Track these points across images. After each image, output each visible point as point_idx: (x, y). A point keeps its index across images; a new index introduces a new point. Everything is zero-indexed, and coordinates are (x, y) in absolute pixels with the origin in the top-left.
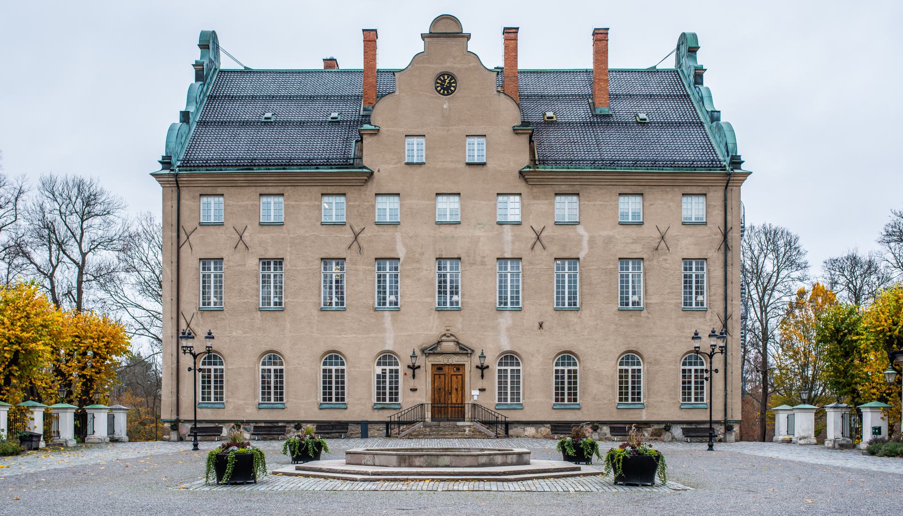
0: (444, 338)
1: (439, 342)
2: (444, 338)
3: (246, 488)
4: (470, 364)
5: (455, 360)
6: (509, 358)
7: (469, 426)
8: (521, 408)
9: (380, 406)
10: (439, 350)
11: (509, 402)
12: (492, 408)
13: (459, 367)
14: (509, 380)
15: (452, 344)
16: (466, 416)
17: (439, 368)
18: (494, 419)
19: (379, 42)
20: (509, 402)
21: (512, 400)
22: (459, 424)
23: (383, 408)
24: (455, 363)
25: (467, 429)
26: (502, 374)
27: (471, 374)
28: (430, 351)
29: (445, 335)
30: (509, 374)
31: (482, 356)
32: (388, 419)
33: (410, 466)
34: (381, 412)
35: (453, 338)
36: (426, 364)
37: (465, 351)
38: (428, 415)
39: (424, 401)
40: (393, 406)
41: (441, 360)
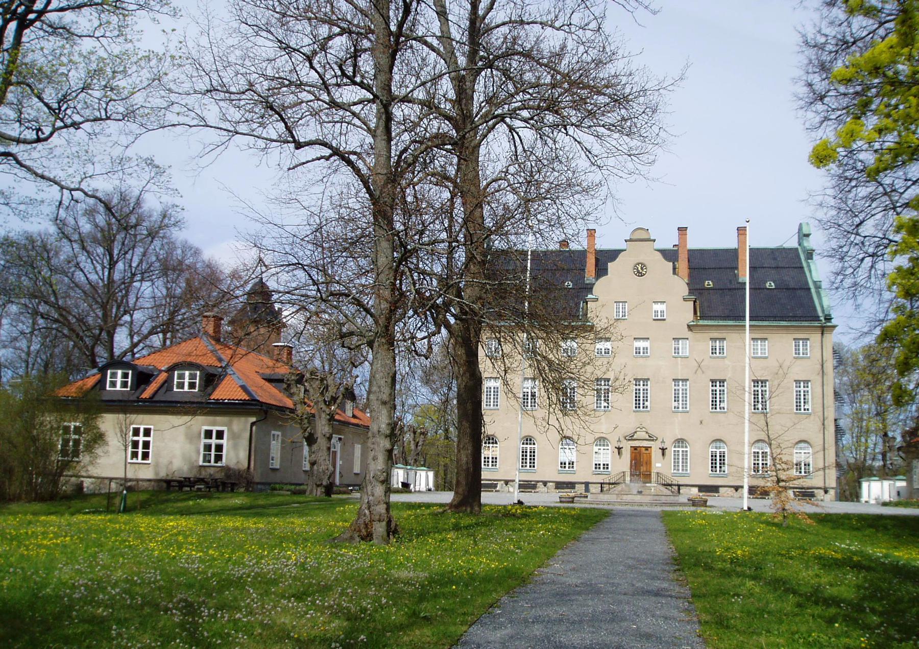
4: (655, 447)
5: (646, 444)
6: (680, 442)
10: (635, 437)
13: (647, 448)
14: (681, 457)
27: (656, 454)
28: (631, 438)
31: (663, 442)
36: (627, 446)
37: (651, 438)
38: (628, 478)
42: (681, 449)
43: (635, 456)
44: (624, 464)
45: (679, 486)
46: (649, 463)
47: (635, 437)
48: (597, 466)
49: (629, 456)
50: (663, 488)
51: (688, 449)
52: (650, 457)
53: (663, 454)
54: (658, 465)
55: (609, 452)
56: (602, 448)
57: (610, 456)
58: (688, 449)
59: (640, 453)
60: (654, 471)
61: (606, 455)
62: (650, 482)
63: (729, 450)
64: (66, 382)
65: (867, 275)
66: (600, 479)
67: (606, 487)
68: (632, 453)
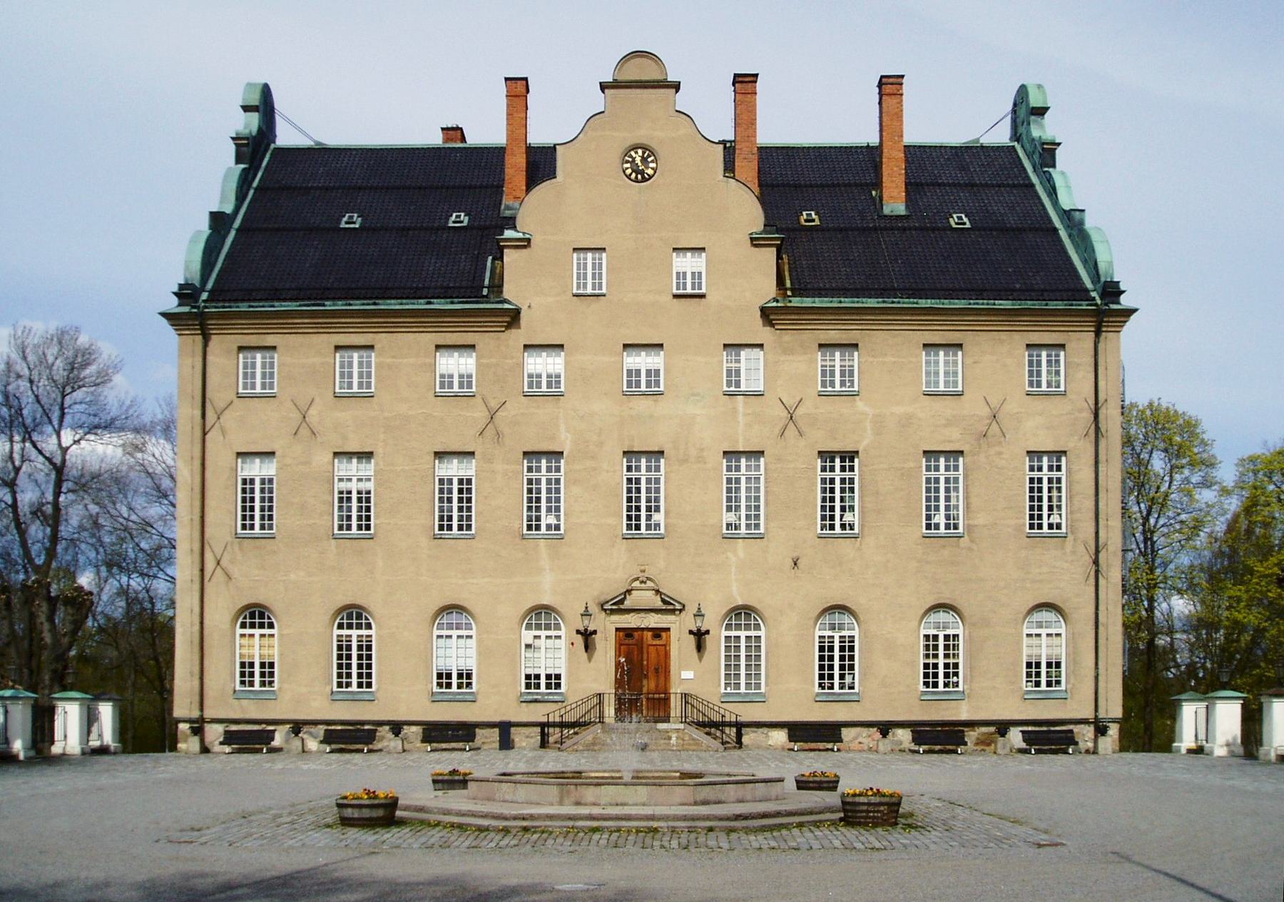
0: (636, 584)
1: (629, 591)
2: (636, 584)
4: (679, 627)
5: (653, 621)
6: (742, 614)
10: (628, 604)
11: (743, 690)
13: (658, 632)
14: (743, 653)
16: (672, 714)
17: (626, 634)
20: (743, 690)
21: (748, 685)
22: (661, 726)
23: (536, 701)
27: (681, 645)
28: (617, 606)
29: (637, 579)
30: (743, 644)
31: (699, 614)
35: (649, 584)
36: (606, 627)
37: (670, 606)
38: (610, 711)
42: (743, 634)
44: (598, 676)
45: (740, 726)
46: (663, 670)
47: (628, 604)
50: (699, 735)
51: (762, 633)
52: (667, 655)
53: (700, 647)
54: (687, 674)
55: (562, 643)
56: (543, 633)
57: (563, 654)
58: (762, 633)
59: (640, 645)
60: (676, 689)
62: (666, 719)
66: (538, 713)
67: (554, 734)
68: (619, 645)
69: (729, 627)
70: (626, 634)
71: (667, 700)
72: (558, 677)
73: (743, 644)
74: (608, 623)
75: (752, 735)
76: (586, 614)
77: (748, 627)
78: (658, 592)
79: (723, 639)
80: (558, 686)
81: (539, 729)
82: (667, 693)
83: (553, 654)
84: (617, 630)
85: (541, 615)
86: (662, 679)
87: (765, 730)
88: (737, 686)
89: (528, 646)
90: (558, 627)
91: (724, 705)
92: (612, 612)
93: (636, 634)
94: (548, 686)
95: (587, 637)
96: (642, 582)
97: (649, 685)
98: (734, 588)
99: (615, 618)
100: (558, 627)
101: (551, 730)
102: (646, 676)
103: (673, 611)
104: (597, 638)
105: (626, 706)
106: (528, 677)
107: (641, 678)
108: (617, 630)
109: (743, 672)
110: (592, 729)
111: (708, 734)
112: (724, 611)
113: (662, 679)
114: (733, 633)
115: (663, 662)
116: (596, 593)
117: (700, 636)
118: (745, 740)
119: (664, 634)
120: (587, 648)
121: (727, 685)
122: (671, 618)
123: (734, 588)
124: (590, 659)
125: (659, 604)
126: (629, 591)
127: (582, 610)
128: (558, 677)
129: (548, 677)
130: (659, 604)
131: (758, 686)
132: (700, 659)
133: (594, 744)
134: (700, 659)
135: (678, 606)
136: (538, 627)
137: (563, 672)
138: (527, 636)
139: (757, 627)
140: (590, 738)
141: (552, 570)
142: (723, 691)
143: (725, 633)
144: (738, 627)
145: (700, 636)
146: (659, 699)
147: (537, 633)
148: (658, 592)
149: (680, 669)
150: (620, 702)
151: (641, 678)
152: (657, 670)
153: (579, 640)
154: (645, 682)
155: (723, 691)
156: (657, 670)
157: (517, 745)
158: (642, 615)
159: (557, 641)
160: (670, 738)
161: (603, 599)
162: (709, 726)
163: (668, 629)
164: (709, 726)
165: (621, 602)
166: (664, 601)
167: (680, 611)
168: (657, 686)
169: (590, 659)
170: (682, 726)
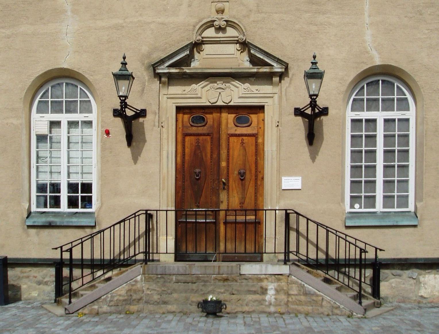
0: (210, 33)
1: (196, 46)
2: (210, 33)
3: (329, 109)
4: (279, 103)
5: (237, 94)
6: (381, 80)
7: (278, 276)
8: (412, 223)
9: (41, 220)
10: (197, 64)
11: (379, 207)
12: (337, 225)
13: (246, 112)
14: (380, 148)
15: (233, 49)
16: (269, 247)
17: (193, 115)
18: (354, 254)
19: (67, 148)
20: (379, 207)
21: (388, 199)
22: (249, 269)
23: (50, 226)
24: (236, 101)
25: (271, 287)
26: (364, 130)
27: (279, 132)
28: (177, 69)
29: (210, 24)
30: (380, 132)
31: (314, 75)
32: (56, 255)
33: (47, 188)
34: (46, 232)
35: (231, 32)
36: (162, 104)
37: (264, 69)
38: (166, 242)
39: (152, 205)
40: (75, 221)
41: (203, 94)
42: (380, 116)
43: (198, 149)
44: (144, 184)
45: (378, 266)
46: (252, 175)
47: (197, 64)
48: (49, 193)
49: (170, 148)
50: (312, 282)
51: (411, 114)
52: (259, 152)
53: (312, 137)
54: (294, 181)
55: (94, 134)
56: (64, 118)
57: (94, 152)
58: (411, 114)
59: (215, 136)
60: (273, 203)
61: (82, 151)
62: (257, 257)
63: (420, 121)
64: (216, 256)
65: (74, 31)
66: (45, 245)
67: (80, 278)
68: (182, 135)
69: (357, 105)
70: (193, 115)
71: (257, 225)
72: (87, 187)
73: (380, 132)
74: (164, 99)
75: (394, 281)
76: (123, 76)
77: (388, 105)
78: (245, 45)
79: (348, 124)
80: (87, 202)
81: (52, 271)
82: (257, 210)
83: (82, 151)
84: (180, 109)
85: (57, 84)
86: (251, 190)
87: (415, 272)
88: (371, 200)
89: (41, 138)
90: (87, 108)
91: (349, 232)
92: (171, 79)
93: (209, 118)
94: (72, 203)
95: (131, 122)
96: (220, 29)
97: (230, 199)
98: (368, 38)
99: (176, 90)
100: (87, 108)
101: (77, 272)
102: (226, 186)
103: (267, 78)
104: (148, 122)
105: (195, 235)
106: (41, 188)
107: (215, 203)
108: (180, 109)
109: (380, 178)
110: (130, 271)
111: (327, 281)
112: (353, 74)
113: (251, 190)
114: (365, 115)
115: (252, 159)
116: (145, 49)
117: (312, 117)
118: (384, 288)
119: (254, 118)
120: (130, 139)
121: (354, 199)
122: (266, 89)
123: (368, 38)
124: (135, 158)
125: (243, 63)
126: (196, 46)
127: (116, 68)
128: (87, 187)
129: (72, 187)
130: (243, 63)
131: (404, 201)
132: (313, 157)
133: (129, 301)
134: (313, 157)
135: (278, 68)
136: (57, 108)
137: (94, 180)
138: (40, 123)
139: (403, 104)
140: (122, 291)
141: (75, 12)
142: (348, 209)
143: (351, 115)
144: (373, 104)
145: (312, 117)
146: (246, 223)
147: (55, 117)
148: (245, 45)
149: (280, 174)
150: (185, 232)
151: (215, 203)
152: (242, 176)
153: (118, 126)
154: (223, 196)
155: (348, 209)
156: (242, 176)
157: (24, 296)
158: (220, 84)
159: (87, 130)
160: (264, 291)
161: (157, 56)
162: (327, 266)
163: (261, 109)
164: (327, 266)
165: (187, 61)
166: (254, 61)
167: (282, 76)
168: (242, 203)
169: (135, 158)
170: (285, 269)
